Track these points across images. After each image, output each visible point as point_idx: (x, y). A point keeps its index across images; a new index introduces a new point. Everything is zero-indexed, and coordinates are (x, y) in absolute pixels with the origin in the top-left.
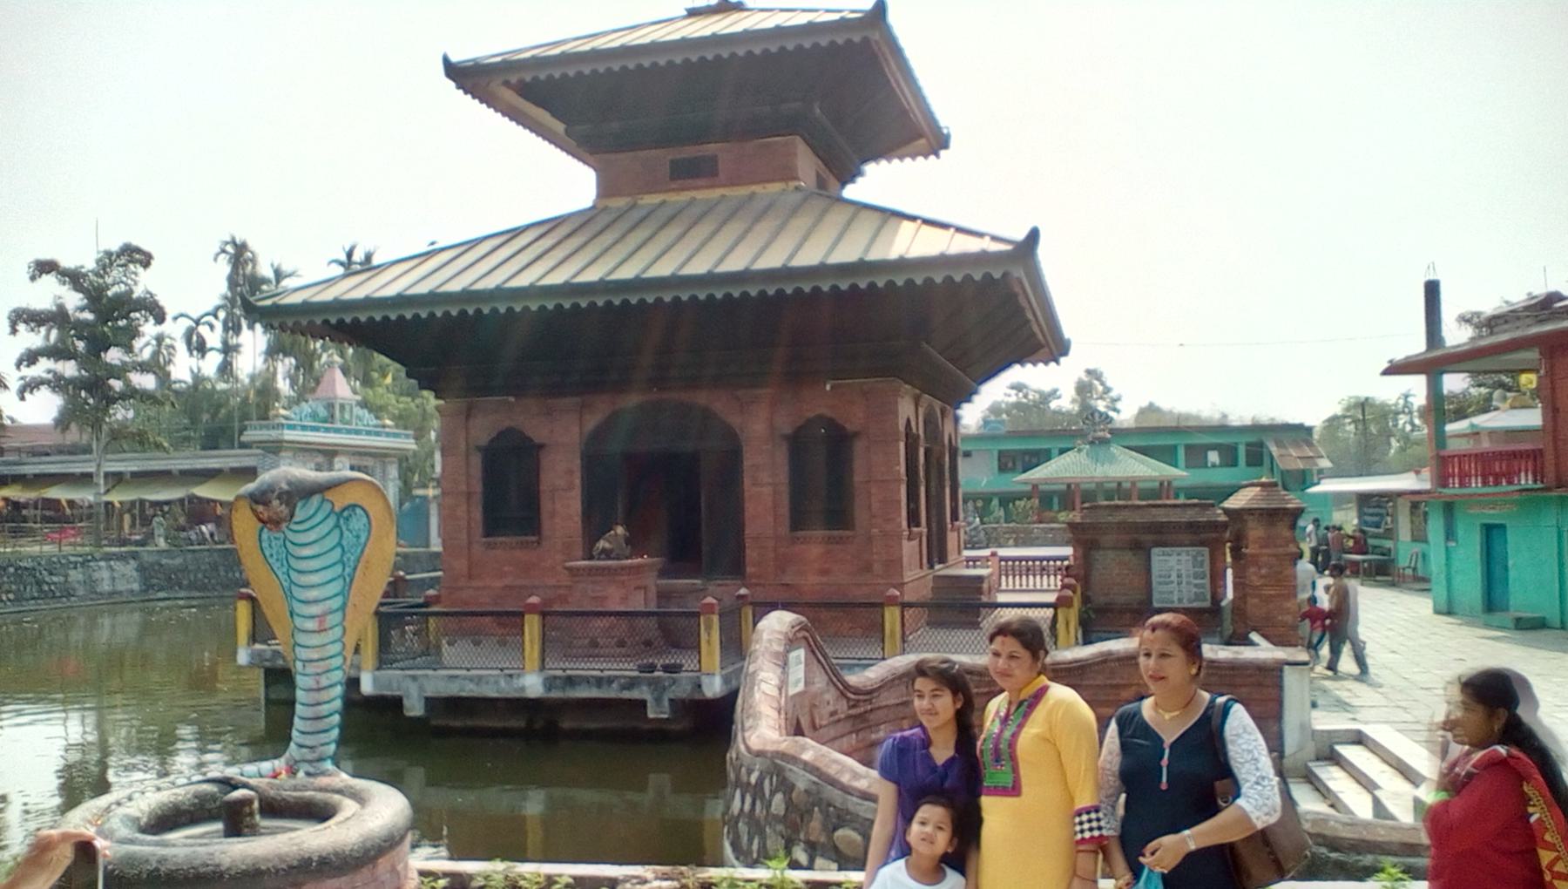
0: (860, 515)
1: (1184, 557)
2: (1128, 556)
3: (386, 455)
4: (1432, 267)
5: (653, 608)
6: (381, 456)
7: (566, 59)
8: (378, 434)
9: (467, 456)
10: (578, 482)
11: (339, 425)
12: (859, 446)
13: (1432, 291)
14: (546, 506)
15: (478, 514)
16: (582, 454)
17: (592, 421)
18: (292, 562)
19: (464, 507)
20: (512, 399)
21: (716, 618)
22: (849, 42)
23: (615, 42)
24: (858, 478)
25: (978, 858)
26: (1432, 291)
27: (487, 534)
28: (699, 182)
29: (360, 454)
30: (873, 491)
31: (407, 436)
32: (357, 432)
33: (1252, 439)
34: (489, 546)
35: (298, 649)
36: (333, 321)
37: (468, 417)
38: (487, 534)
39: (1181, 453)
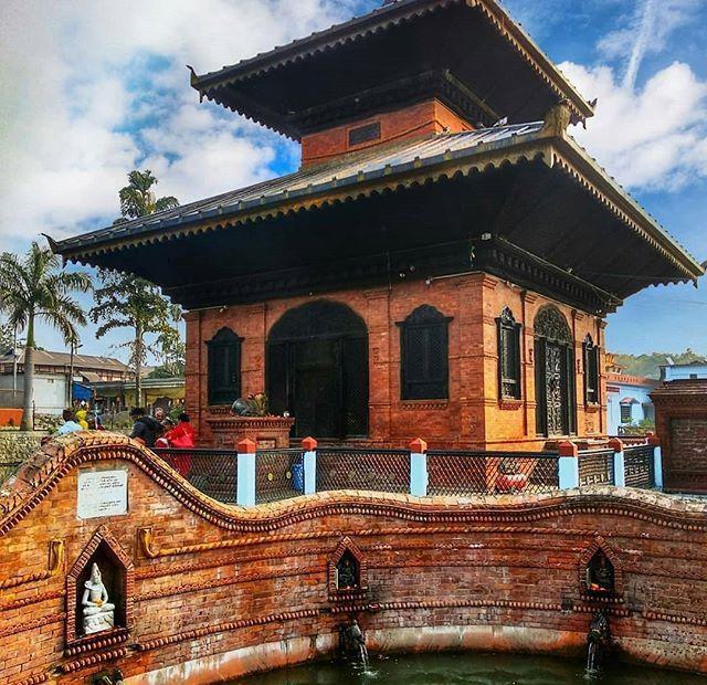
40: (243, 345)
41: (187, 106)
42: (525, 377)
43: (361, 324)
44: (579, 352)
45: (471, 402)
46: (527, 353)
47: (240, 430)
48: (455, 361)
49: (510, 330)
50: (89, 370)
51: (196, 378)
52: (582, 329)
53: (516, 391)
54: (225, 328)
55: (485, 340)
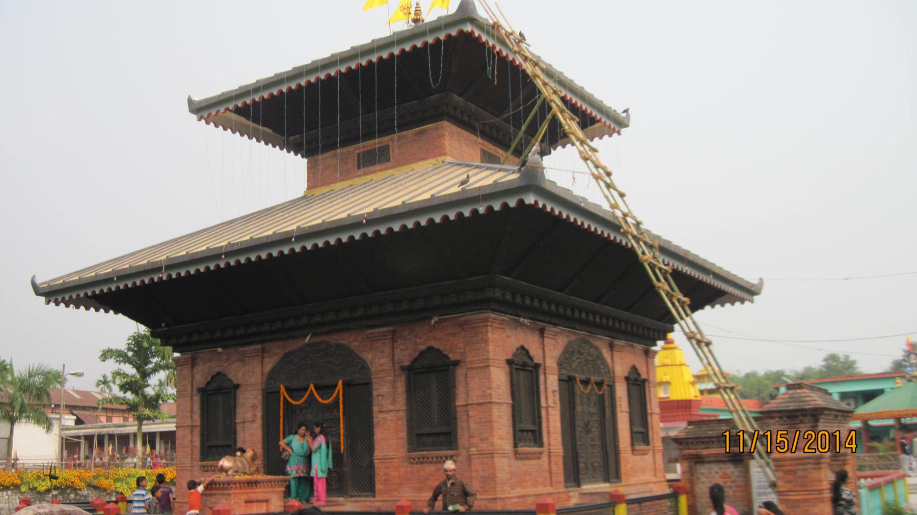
0: (463, 439)
9: (192, 397)
10: (259, 414)
12: (460, 372)
14: (461, 425)
16: (263, 390)
17: (270, 363)
19: (189, 437)
20: (220, 350)
22: (360, 66)
23: (647, 395)
24: (460, 402)
25: (346, 175)
27: (202, 460)
30: (471, 413)
37: (193, 366)
38: (202, 460)
40: (239, 392)
41: (9, 425)
42: (548, 421)
43: (364, 368)
44: (621, 391)
45: (482, 453)
46: (550, 394)
47: (226, 492)
48: (463, 409)
49: (524, 369)
50: (84, 408)
51: (188, 431)
52: (620, 362)
53: (536, 437)
54: (219, 374)
55: (494, 385)
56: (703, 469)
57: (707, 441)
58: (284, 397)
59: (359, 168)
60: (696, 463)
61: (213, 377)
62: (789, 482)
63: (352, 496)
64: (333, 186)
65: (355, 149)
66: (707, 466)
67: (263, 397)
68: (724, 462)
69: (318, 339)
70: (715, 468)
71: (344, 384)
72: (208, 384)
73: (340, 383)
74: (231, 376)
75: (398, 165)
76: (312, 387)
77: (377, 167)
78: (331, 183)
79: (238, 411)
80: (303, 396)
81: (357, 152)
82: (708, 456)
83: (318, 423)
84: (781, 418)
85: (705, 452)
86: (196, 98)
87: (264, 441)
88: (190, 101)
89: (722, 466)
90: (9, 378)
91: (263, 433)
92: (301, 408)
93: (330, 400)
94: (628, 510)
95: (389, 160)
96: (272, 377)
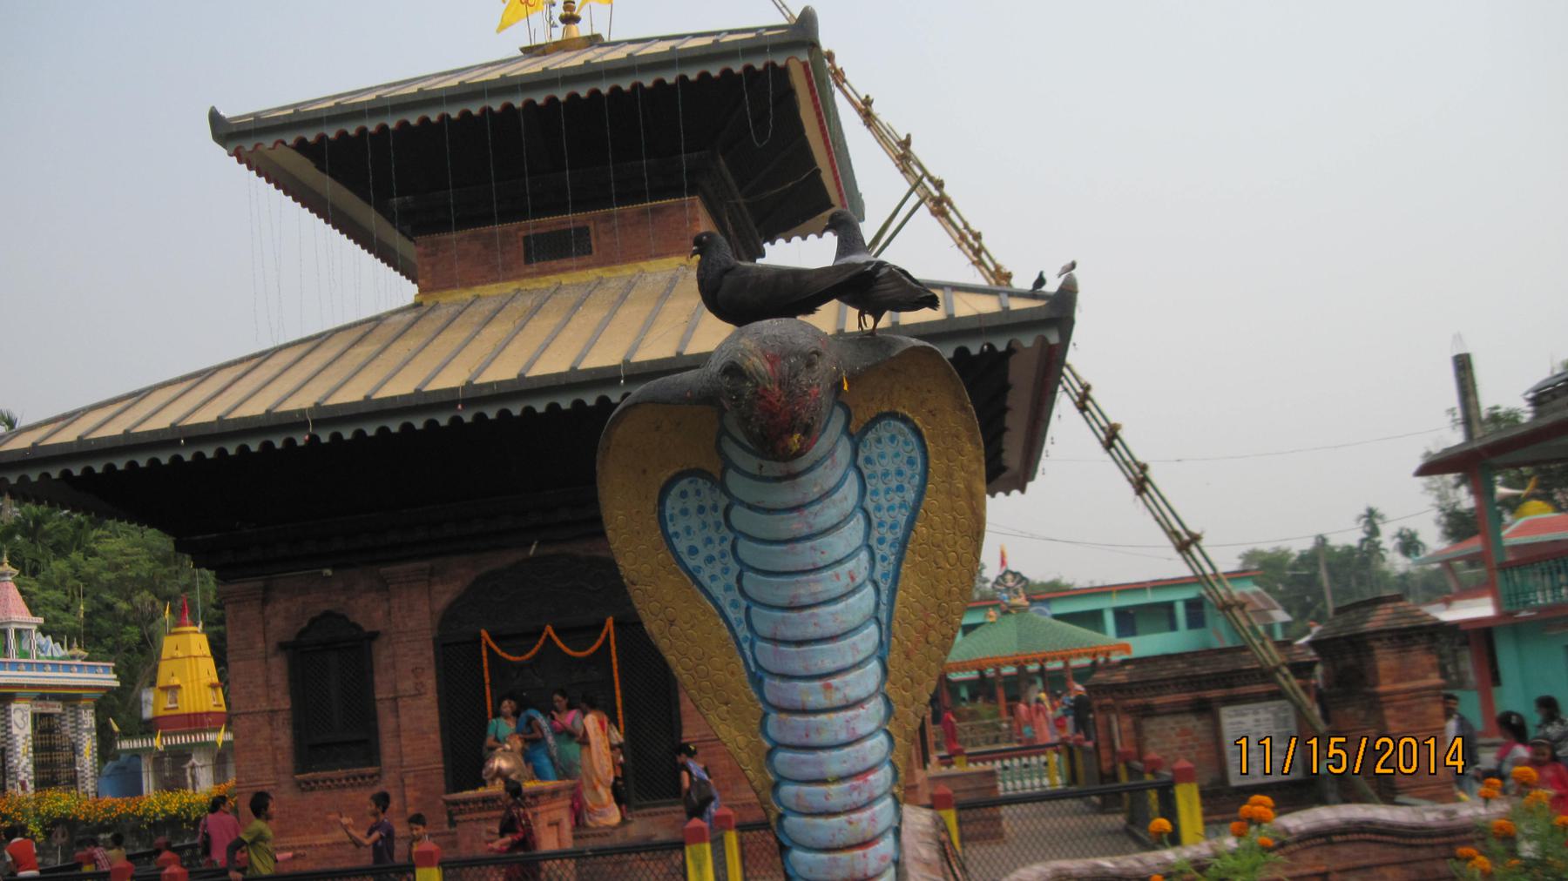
1: (1263, 716)
2: (1193, 723)
3: (78, 698)
4: (1458, 338)
5: (569, 845)
6: (70, 697)
7: (379, 108)
8: (68, 668)
10: (430, 682)
11: (13, 658)
13: (1463, 365)
14: (386, 723)
15: (285, 738)
17: (444, 595)
18: (745, 548)
20: (328, 572)
21: (732, 838)
26: (1463, 365)
28: (566, 263)
29: (42, 697)
31: (106, 669)
32: (41, 666)
33: (1190, 594)
34: (305, 787)
35: (782, 756)
36: (77, 471)
37: (265, 602)
39: (1109, 620)
56: (1151, 725)
57: (1159, 686)
58: (489, 648)
59: (528, 261)
60: (1144, 716)
61: (313, 621)
62: (1401, 721)
63: (641, 807)
64: (478, 290)
65: (520, 229)
66: (1157, 720)
67: (436, 654)
68: (1182, 712)
69: (551, 550)
70: (1170, 722)
71: (615, 623)
72: (302, 633)
73: (610, 621)
74: (357, 618)
75: (608, 261)
76: (549, 629)
77: (574, 262)
78: (477, 284)
79: (377, 679)
80: (532, 647)
81: (522, 234)
82: (1161, 706)
83: (546, 689)
84: (1390, 639)
85: (1158, 701)
86: (226, 112)
87: (443, 729)
88: (215, 118)
89: (1180, 718)
90: (977, 596)
91: (441, 714)
92: (520, 667)
93: (528, 655)
94: (445, 877)
95: (590, 252)
96: (449, 617)
